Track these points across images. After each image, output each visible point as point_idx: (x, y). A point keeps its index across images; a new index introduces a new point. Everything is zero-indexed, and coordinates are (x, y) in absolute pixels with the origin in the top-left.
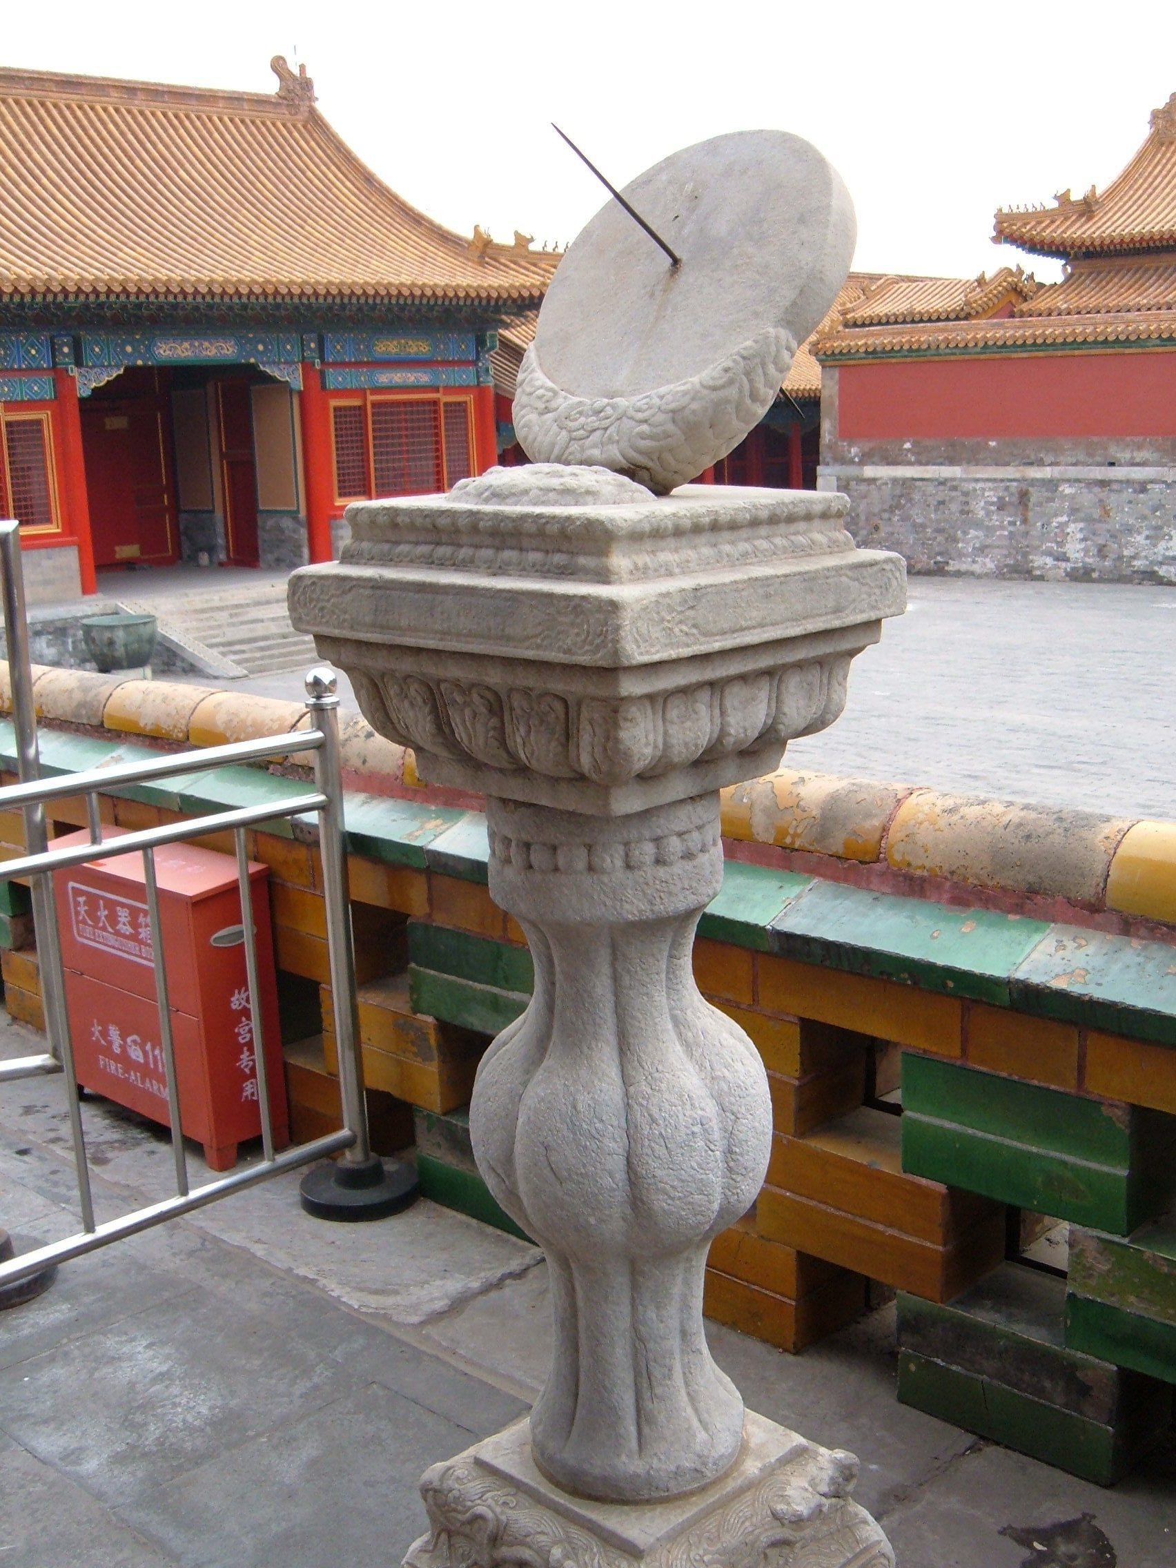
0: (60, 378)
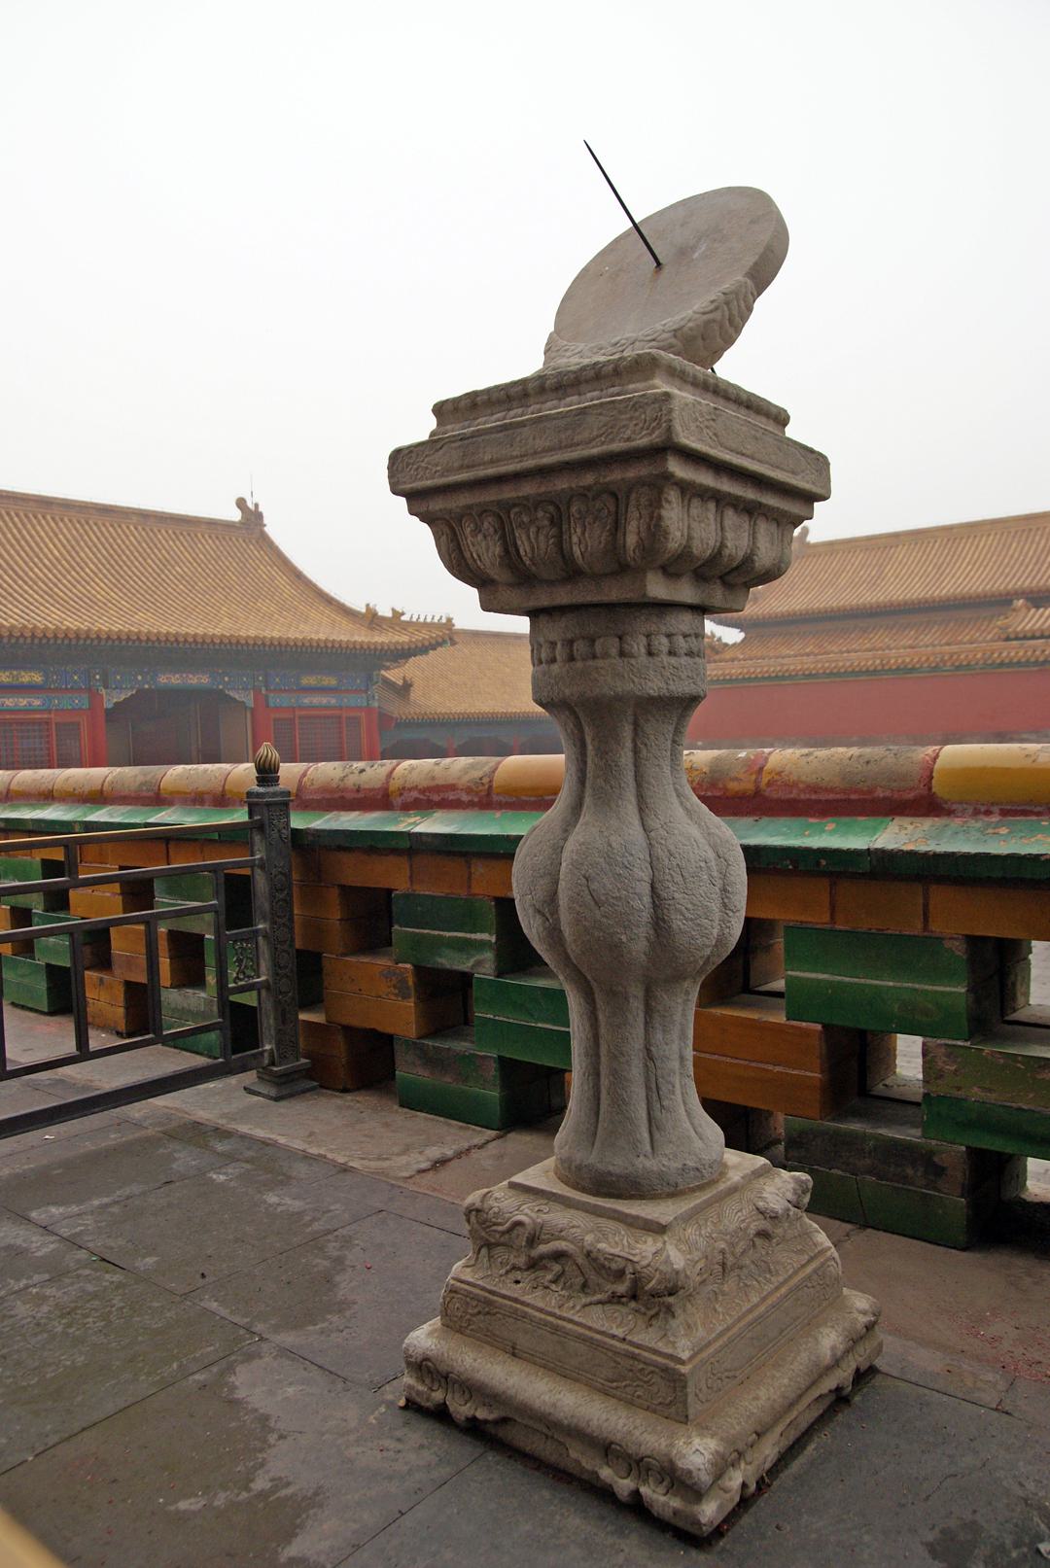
0: (94, 696)
